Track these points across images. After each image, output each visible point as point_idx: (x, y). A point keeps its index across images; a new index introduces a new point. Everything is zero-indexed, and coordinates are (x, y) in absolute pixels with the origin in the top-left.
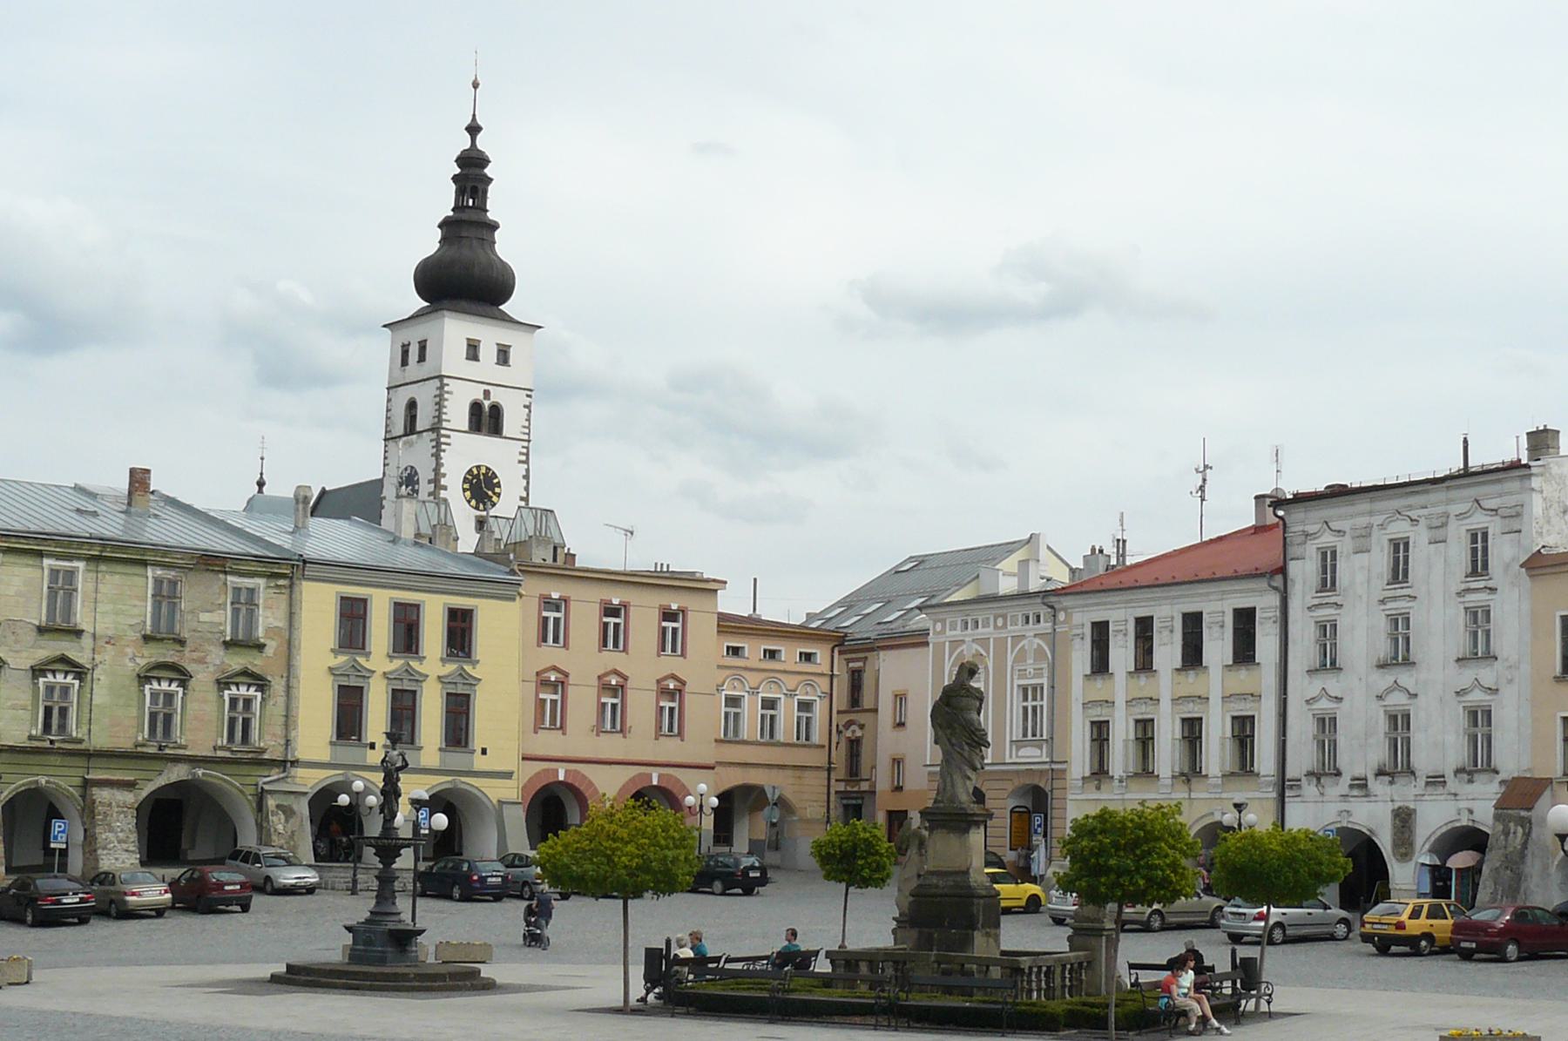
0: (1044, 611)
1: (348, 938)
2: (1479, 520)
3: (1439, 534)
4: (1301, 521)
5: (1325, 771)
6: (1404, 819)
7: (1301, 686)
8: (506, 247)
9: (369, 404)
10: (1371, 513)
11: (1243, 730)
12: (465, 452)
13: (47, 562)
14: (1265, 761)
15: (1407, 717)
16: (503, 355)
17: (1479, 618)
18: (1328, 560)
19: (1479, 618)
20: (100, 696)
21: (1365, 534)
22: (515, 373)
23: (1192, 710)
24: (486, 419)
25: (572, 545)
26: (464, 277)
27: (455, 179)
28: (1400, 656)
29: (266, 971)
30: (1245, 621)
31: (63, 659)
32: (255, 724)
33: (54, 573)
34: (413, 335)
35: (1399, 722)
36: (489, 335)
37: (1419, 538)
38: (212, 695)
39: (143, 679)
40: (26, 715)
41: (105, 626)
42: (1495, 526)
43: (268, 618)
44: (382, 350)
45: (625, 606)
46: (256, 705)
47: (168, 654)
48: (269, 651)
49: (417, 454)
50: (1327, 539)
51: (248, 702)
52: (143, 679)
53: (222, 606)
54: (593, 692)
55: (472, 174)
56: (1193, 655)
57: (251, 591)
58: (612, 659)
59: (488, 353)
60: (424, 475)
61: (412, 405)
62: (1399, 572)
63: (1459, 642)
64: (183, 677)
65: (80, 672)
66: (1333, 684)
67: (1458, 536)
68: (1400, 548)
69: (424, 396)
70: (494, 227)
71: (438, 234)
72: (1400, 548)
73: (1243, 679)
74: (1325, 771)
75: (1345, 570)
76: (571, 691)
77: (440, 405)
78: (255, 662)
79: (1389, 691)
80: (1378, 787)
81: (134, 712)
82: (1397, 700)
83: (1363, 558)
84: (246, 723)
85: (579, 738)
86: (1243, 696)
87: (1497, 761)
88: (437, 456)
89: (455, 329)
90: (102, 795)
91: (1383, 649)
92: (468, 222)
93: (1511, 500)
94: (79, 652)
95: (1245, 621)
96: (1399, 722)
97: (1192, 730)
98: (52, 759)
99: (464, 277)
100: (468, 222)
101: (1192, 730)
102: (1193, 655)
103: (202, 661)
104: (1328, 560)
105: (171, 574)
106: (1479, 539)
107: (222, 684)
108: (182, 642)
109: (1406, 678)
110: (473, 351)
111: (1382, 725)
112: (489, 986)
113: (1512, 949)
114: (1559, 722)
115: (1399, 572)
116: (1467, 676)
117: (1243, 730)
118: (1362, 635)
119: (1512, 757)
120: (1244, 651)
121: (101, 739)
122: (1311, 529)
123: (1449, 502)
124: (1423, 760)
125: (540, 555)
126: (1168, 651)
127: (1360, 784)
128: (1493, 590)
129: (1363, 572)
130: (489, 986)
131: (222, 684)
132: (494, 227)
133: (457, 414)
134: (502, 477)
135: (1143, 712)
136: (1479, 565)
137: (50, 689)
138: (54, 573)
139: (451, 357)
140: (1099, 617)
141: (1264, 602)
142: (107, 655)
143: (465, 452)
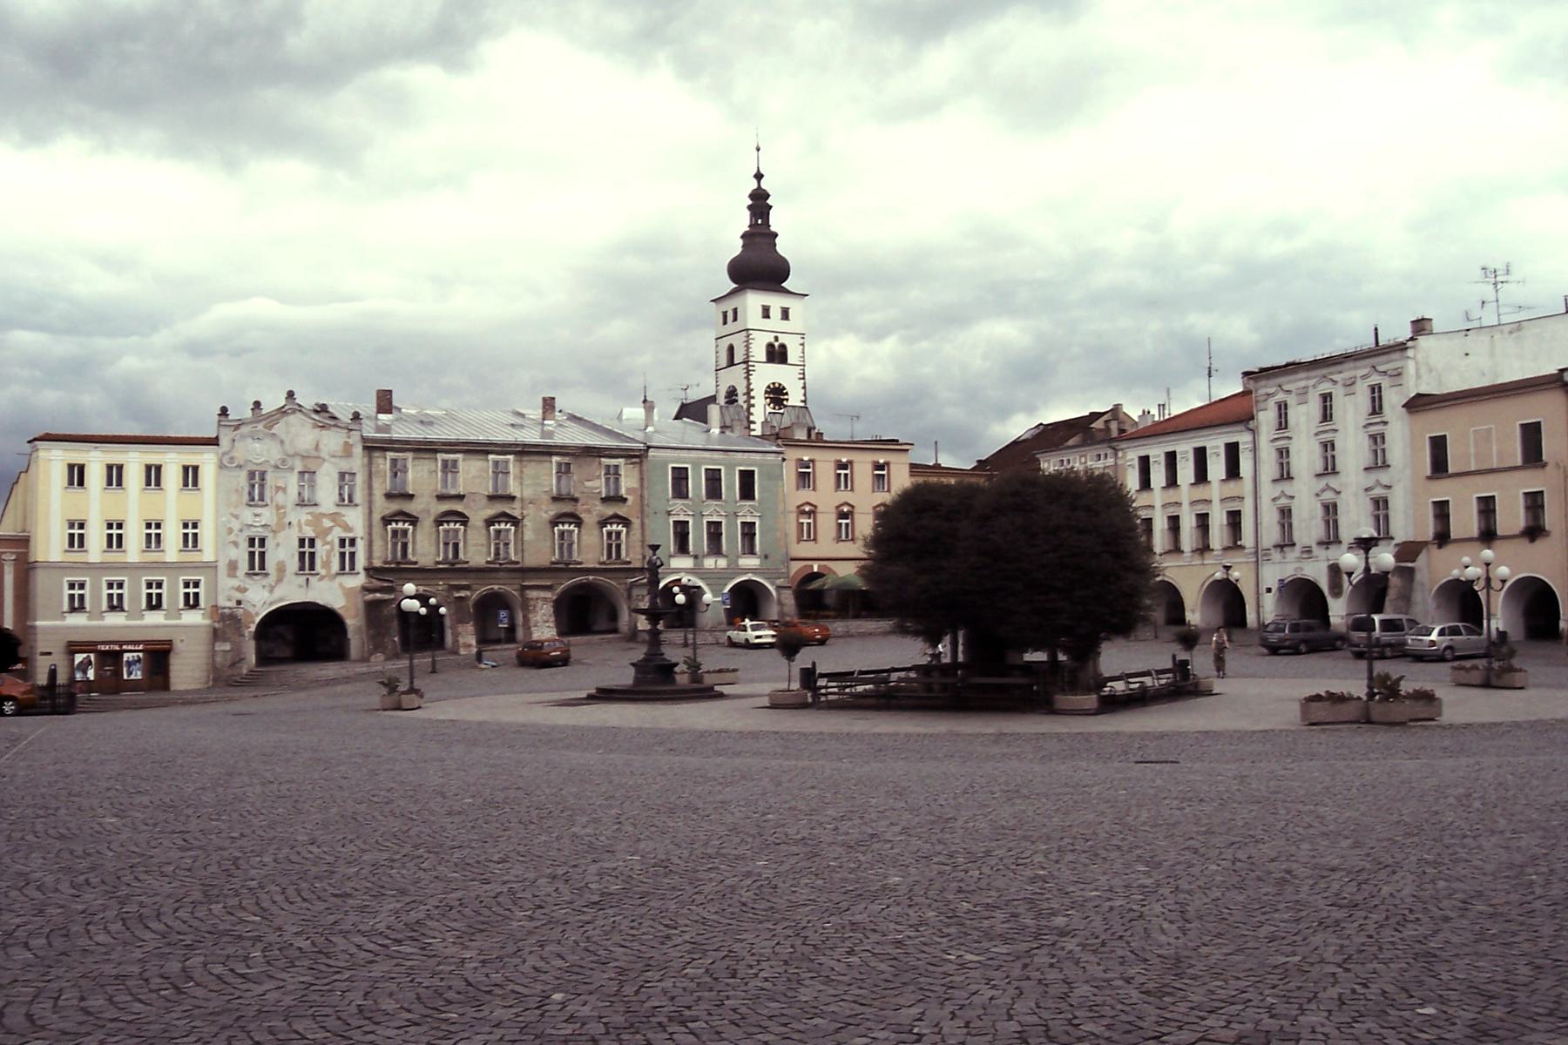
0: (1109, 451)
1: (632, 671)
2: (1375, 379)
3: (1350, 390)
4: (1266, 387)
5: (1286, 544)
6: (1335, 570)
7: (1268, 491)
8: (783, 247)
9: (705, 345)
10: (1308, 378)
11: (1234, 518)
12: (765, 375)
13: (491, 457)
14: (1247, 538)
15: (1335, 506)
16: (785, 314)
17: (1377, 439)
18: (1282, 408)
19: (1377, 439)
20: (528, 535)
21: (1304, 392)
22: (793, 324)
23: (1202, 509)
24: (777, 354)
25: (820, 426)
26: (760, 267)
27: (750, 207)
28: (1330, 469)
29: (584, 694)
30: (1232, 451)
31: (505, 514)
32: (623, 547)
33: (496, 463)
34: (728, 306)
35: (1330, 510)
36: (776, 302)
37: (1338, 393)
38: (596, 532)
39: (554, 523)
40: (485, 550)
41: (528, 493)
42: (1385, 383)
43: (628, 481)
44: (715, 312)
45: (812, 461)
46: (623, 535)
47: (566, 508)
48: (629, 503)
49: (735, 377)
50: (1281, 397)
51: (618, 534)
52: (554, 523)
53: (599, 477)
54: (833, 516)
55: (760, 203)
56: (1201, 476)
57: (617, 467)
58: (805, 495)
59: (776, 313)
60: (741, 390)
61: (731, 348)
62: (1327, 416)
63: (1366, 458)
64: (579, 522)
65: (516, 522)
66: (1286, 487)
67: (1362, 390)
68: (1326, 398)
69: (738, 341)
70: (776, 235)
71: (741, 242)
72: (1326, 398)
73: (1232, 488)
74: (1286, 544)
75: (1294, 414)
76: (819, 516)
77: (748, 347)
78: (621, 511)
79: (1323, 491)
80: (1319, 552)
81: (549, 543)
82: (1328, 496)
83: (1303, 408)
84: (618, 546)
85: (826, 546)
86: (1232, 498)
87: (1393, 532)
88: (748, 378)
89: (754, 301)
90: (533, 594)
91: (1319, 468)
92: (760, 234)
93: (1398, 364)
94: (411, 508)
95: (1232, 451)
96: (1330, 510)
97: (1203, 521)
98: (501, 574)
99: (760, 267)
100: (760, 234)
101: (1203, 521)
102: (1201, 476)
103: (589, 511)
104: (1282, 408)
105: (566, 460)
106: (1376, 391)
107: (603, 523)
108: (576, 500)
109: (1333, 482)
110: (766, 313)
111: (1320, 512)
112: (721, 696)
113: (1303, 648)
114: (1475, 502)
115: (1327, 416)
116: (1372, 478)
117: (1234, 518)
118: (1305, 457)
119: (1402, 529)
120: (1233, 471)
121: (530, 561)
122: (1271, 390)
123: (1356, 368)
124: (1347, 534)
125: (801, 435)
126: (1186, 472)
127: (1308, 551)
128: (1385, 423)
129: (1304, 416)
130: (721, 696)
131: (439, 522)
132: (776, 235)
133: (759, 353)
134: (788, 389)
135: (1172, 511)
136: (1377, 408)
137: (610, 534)
138: (496, 463)
139: (752, 318)
140: (1170, 449)
141: (1244, 439)
142: (530, 511)
143: (765, 375)
